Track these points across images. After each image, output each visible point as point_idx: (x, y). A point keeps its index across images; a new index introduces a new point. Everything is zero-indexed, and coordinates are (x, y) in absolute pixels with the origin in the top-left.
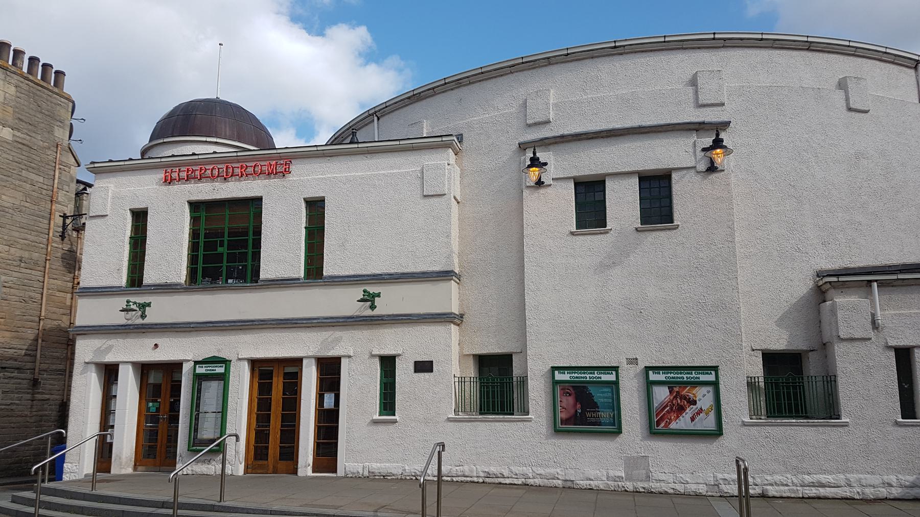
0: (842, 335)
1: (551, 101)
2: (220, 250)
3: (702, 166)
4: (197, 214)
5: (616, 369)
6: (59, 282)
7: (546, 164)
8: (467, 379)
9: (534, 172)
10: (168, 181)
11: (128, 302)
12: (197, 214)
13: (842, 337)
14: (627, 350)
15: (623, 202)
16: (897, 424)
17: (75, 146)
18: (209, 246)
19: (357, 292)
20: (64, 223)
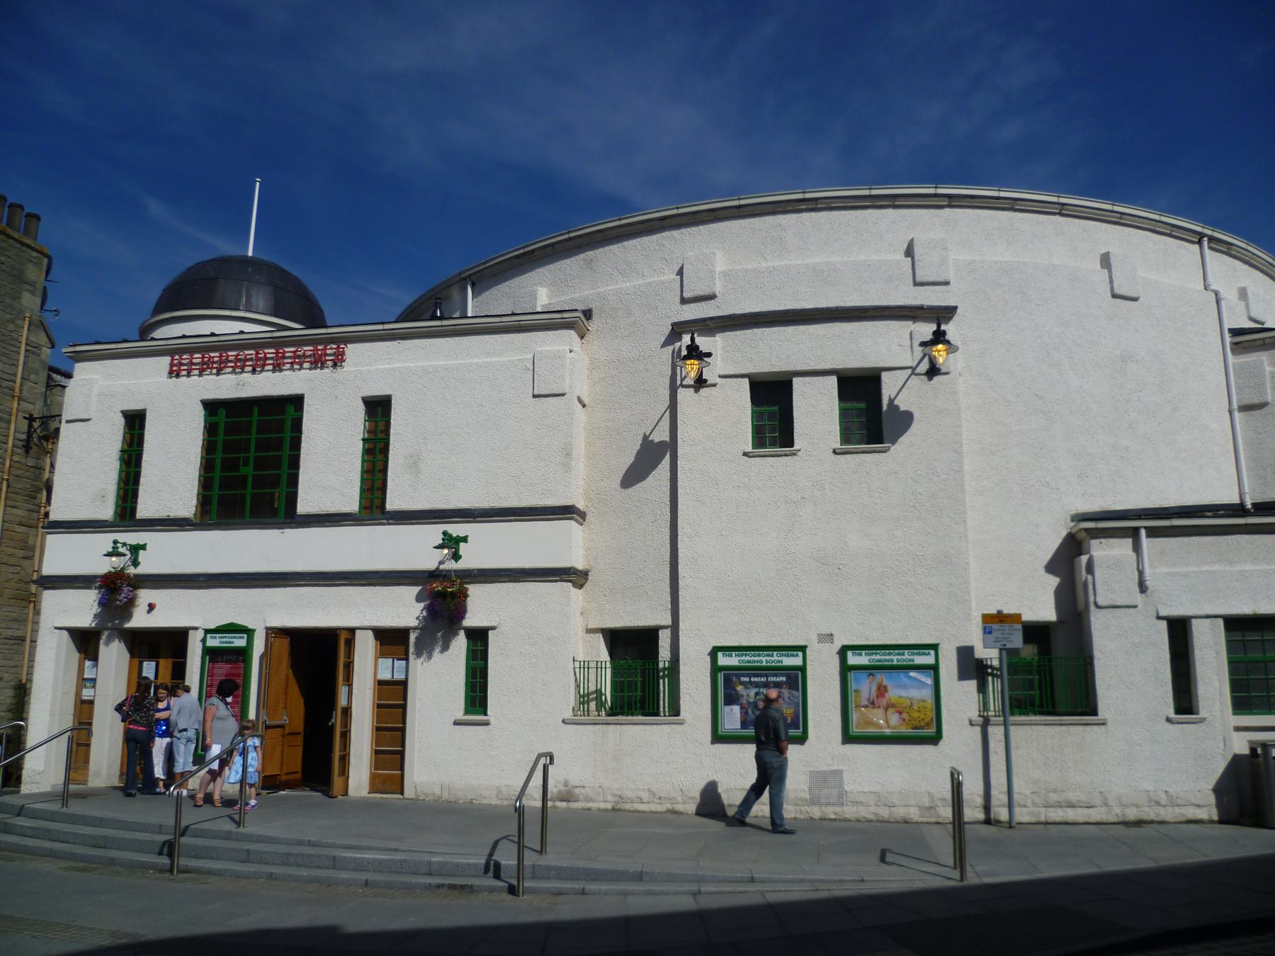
0: (1101, 602)
1: (719, 269)
2: (243, 471)
3: (924, 366)
4: (214, 419)
5: (802, 649)
6: (20, 512)
7: (709, 355)
8: (593, 665)
9: (692, 368)
10: (174, 373)
11: (115, 542)
12: (214, 419)
13: (1100, 603)
14: (816, 622)
15: (817, 409)
16: (1169, 720)
17: (50, 319)
18: (229, 465)
19: (434, 532)
20: (30, 426)
